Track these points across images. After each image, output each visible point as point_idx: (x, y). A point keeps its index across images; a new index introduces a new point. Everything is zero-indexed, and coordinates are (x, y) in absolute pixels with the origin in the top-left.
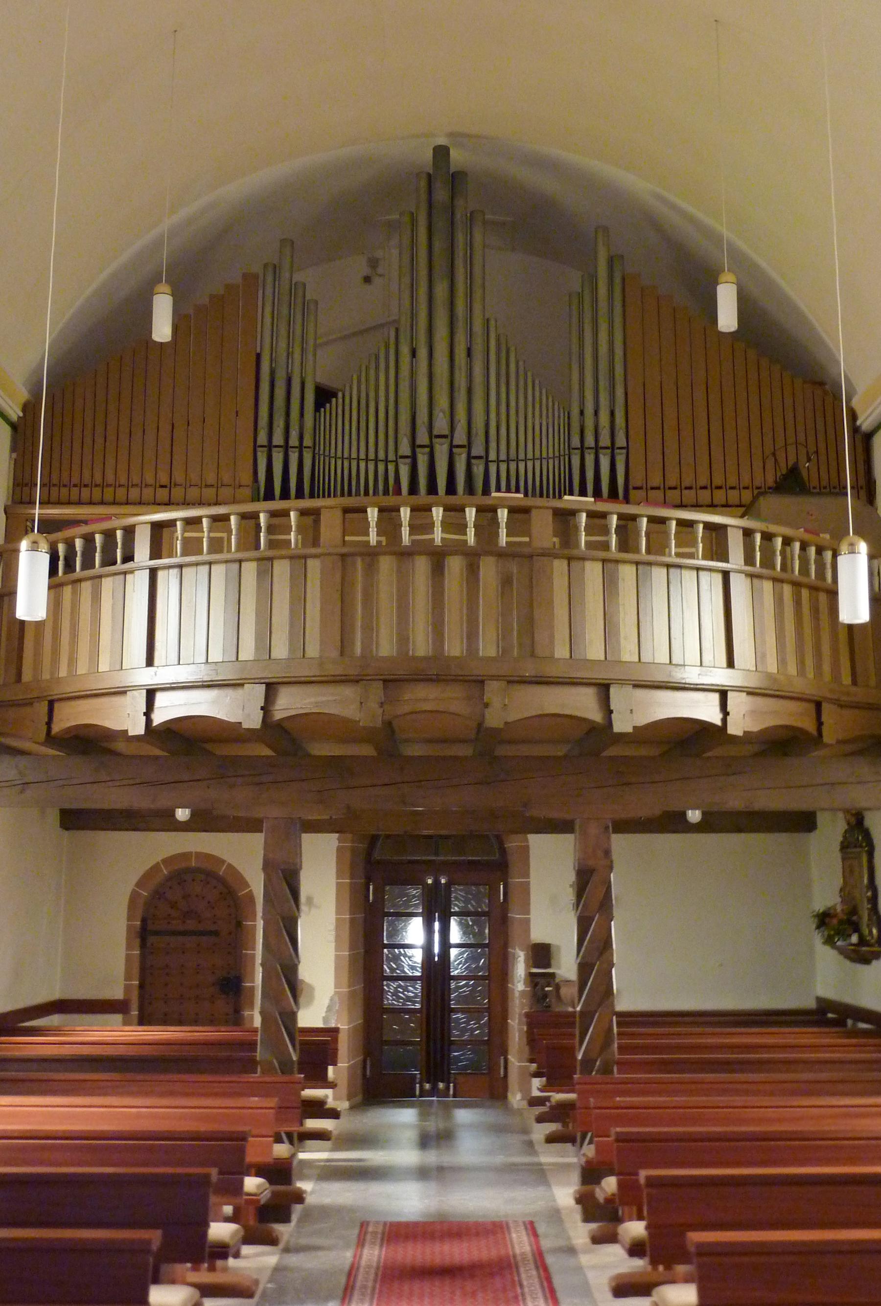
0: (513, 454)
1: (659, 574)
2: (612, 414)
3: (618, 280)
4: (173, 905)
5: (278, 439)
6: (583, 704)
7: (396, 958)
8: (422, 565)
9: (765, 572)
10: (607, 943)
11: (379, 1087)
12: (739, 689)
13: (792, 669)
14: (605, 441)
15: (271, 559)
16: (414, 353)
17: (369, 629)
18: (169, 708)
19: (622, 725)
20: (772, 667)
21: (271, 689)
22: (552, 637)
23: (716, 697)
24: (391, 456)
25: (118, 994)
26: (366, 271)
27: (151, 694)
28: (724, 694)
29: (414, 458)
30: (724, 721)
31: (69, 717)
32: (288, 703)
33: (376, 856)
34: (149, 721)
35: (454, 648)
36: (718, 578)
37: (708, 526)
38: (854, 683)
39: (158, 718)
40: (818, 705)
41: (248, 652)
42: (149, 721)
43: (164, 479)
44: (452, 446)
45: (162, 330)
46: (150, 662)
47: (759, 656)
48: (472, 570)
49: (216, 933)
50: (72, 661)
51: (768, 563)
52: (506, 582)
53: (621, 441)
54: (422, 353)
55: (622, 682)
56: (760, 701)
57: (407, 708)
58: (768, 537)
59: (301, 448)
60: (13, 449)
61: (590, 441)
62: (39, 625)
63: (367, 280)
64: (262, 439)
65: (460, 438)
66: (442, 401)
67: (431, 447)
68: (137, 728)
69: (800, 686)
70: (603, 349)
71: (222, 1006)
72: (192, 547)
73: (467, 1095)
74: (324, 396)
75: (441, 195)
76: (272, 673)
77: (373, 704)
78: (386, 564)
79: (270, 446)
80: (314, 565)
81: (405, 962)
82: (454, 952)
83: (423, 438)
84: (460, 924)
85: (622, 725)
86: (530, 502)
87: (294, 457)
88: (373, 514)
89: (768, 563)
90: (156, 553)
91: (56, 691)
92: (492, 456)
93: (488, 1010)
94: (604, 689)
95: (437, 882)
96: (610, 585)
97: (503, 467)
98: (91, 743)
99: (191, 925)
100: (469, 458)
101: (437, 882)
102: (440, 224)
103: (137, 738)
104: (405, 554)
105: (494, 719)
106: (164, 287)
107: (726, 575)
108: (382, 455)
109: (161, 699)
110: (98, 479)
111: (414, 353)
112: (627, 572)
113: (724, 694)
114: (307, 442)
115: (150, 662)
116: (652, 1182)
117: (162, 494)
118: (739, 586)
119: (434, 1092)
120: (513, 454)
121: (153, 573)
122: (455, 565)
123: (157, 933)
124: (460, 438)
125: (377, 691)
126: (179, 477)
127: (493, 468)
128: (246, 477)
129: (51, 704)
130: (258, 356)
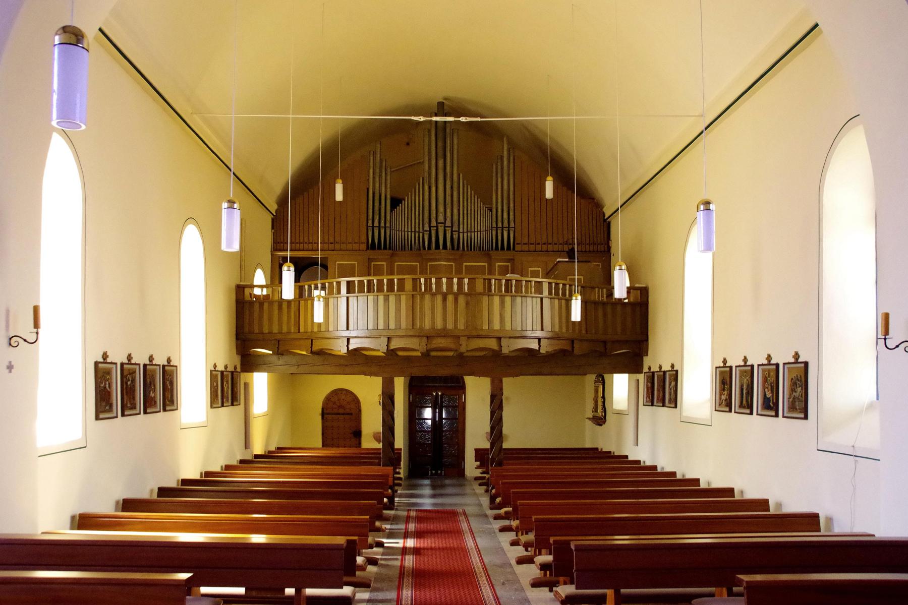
1: (519, 299)
3: (512, 158)
4: (334, 403)
5: (376, 224)
6: (492, 344)
7: (421, 424)
8: (439, 298)
11: (416, 472)
12: (545, 338)
13: (564, 330)
14: (506, 224)
16: (430, 188)
17: (422, 319)
19: (505, 351)
20: (557, 329)
21: (389, 339)
27: (348, 340)
29: (430, 231)
32: (395, 344)
35: (450, 326)
36: (539, 300)
39: (351, 348)
40: (573, 342)
41: (381, 326)
43: (332, 240)
46: (348, 329)
47: (552, 325)
48: (456, 300)
51: (557, 293)
52: (467, 303)
53: (512, 225)
55: (505, 337)
56: (553, 341)
59: (385, 227)
60: (273, 228)
61: (500, 225)
62: (289, 302)
63: (408, 144)
65: (448, 223)
66: (441, 209)
67: (437, 227)
68: (344, 350)
70: (505, 187)
72: (361, 291)
73: (447, 476)
78: (428, 297)
79: (373, 227)
81: (425, 425)
83: (434, 223)
85: (505, 351)
86: (475, 276)
87: (382, 231)
89: (557, 293)
90: (348, 292)
92: (461, 230)
94: (499, 339)
95: (437, 394)
96: (502, 303)
97: (465, 235)
99: (341, 411)
100: (452, 231)
101: (437, 394)
102: (441, 135)
104: (433, 295)
105: (463, 349)
106: (340, 181)
107: (542, 299)
109: (351, 341)
111: (430, 188)
112: (508, 299)
113: (539, 339)
114: (388, 225)
115: (348, 329)
116: (513, 493)
118: (546, 302)
119: (436, 474)
122: (450, 298)
123: (328, 414)
124: (448, 223)
125: (425, 340)
126: (337, 239)
128: (364, 239)
130: (368, 189)
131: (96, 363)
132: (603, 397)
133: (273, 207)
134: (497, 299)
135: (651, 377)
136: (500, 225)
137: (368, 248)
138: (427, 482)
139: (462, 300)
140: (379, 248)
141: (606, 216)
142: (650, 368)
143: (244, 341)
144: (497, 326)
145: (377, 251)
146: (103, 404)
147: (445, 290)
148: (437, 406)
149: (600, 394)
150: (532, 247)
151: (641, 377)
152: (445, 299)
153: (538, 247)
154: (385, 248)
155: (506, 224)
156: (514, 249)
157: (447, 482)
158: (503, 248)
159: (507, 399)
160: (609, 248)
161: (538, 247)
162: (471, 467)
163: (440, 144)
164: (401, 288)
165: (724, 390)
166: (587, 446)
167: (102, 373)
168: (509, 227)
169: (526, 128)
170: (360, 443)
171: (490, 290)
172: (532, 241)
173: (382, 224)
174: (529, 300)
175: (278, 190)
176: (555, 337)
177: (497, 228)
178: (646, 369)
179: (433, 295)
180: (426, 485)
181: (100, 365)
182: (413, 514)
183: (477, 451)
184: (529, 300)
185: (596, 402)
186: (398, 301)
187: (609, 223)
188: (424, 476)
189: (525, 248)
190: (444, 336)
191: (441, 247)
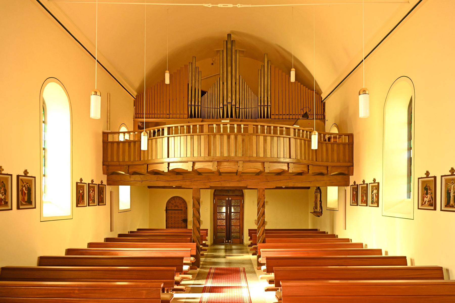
0: (245, 107)
2: (268, 98)
5: (193, 103)
8: (225, 137)
9: (298, 138)
10: (264, 213)
11: (217, 241)
12: (292, 163)
14: (266, 104)
15: (193, 135)
16: (223, 83)
18: (172, 167)
21: (194, 163)
22: (252, 152)
23: (286, 164)
24: (218, 107)
26: (212, 62)
27: (169, 164)
28: (288, 164)
30: (288, 169)
31: (151, 168)
32: (197, 166)
33: (216, 194)
34: (168, 169)
35: (233, 155)
36: (288, 139)
37: (286, 128)
38: (316, 161)
39: (170, 169)
40: (308, 166)
42: (168, 169)
44: (232, 105)
45: (167, 81)
46: (168, 157)
47: (296, 155)
49: (182, 210)
50: (152, 156)
51: (299, 136)
52: (243, 140)
53: (269, 104)
54: (225, 84)
57: (223, 167)
58: (299, 130)
60: (134, 106)
61: (262, 104)
63: (212, 64)
64: (190, 103)
65: (234, 103)
66: (230, 95)
67: (227, 105)
68: (166, 171)
69: (305, 161)
71: (183, 225)
72: (176, 133)
73: (234, 244)
74: (203, 93)
75: (229, 46)
76: (194, 160)
77: (215, 166)
78: (218, 137)
79: (191, 105)
80: (202, 137)
82: (232, 214)
83: (225, 103)
84: (234, 208)
88: (215, 126)
89: (299, 136)
90: (169, 134)
91: (148, 162)
92: (241, 107)
93: (239, 226)
94: (263, 163)
95: (229, 199)
96: (265, 141)
97: (243, 110)
98: (157, 173)
99: (176, 208)
100: (236, 108)
103: (166, 173)
104: (222, 135)
106: (168, 72)
107: (290, 138)
108: (216, 107)
110: (153, 113)
111: (223, 83)
112: (269, 138)
113: (288, 164)
114: (200, 104)
115: (168, 157)
117: (168, 116)
118: (293, 141)
119: (228, 242)
120: (245, 107)
121: (168, 138)
122: (232, 137)
123: (169, 210)
124: (234, 103)
126: (171, 112)
127: (241, 110)
128: (186, 112)
129: (148, 165)
130: (188, 84)
131: (77, 183)
132: (321, 201)
133: (135, 94)
134: (261, 138)
135: (355, 189)
136: (262, 104)
137: (188, 117)
138: (223, 247)
139: (240, 138)
140: (195, 117)
141: (323, 96)
142: (355, 182)
143: (108, 166)
144: (262, 155)
145: (193, 119)
146: (79, 200)
147: (229, 132)
148: (229, 205)
149: (319, 199)
150: (281, 117)
151: (348, 189)
152: (229, 137)
153: (284, 117)
154: (198, 117)
155: (266, 104)
156: (270, 118)
157: (234, 247)
158: (264, 117)
160: (324, 116)
161: (284, 117)
162: (247, 240)
163: (229, 58)
164: (202, 131)
166: (310, 228)
167: (79, 187)
168: (268, 105)
169: (278, 51)
170: (187, 226)
171: (257, 132)
172: (281, 113)
173: (196, 104)
174: (282, 139)
175: (137, 85)
176: (297, 163)
177: (261, 106)
178: (351, 183)
179: (222, 135)
180: (222, 249)
181: (79, 184)
182: (213, 271)
183: (249, 230)
184: (282, 139)
185: (316, 204)
186: (199, 140)
187: (324, 103)
188: (221, 243)
189: (277, 117)
190: (228, 161)
191: (229, 116)
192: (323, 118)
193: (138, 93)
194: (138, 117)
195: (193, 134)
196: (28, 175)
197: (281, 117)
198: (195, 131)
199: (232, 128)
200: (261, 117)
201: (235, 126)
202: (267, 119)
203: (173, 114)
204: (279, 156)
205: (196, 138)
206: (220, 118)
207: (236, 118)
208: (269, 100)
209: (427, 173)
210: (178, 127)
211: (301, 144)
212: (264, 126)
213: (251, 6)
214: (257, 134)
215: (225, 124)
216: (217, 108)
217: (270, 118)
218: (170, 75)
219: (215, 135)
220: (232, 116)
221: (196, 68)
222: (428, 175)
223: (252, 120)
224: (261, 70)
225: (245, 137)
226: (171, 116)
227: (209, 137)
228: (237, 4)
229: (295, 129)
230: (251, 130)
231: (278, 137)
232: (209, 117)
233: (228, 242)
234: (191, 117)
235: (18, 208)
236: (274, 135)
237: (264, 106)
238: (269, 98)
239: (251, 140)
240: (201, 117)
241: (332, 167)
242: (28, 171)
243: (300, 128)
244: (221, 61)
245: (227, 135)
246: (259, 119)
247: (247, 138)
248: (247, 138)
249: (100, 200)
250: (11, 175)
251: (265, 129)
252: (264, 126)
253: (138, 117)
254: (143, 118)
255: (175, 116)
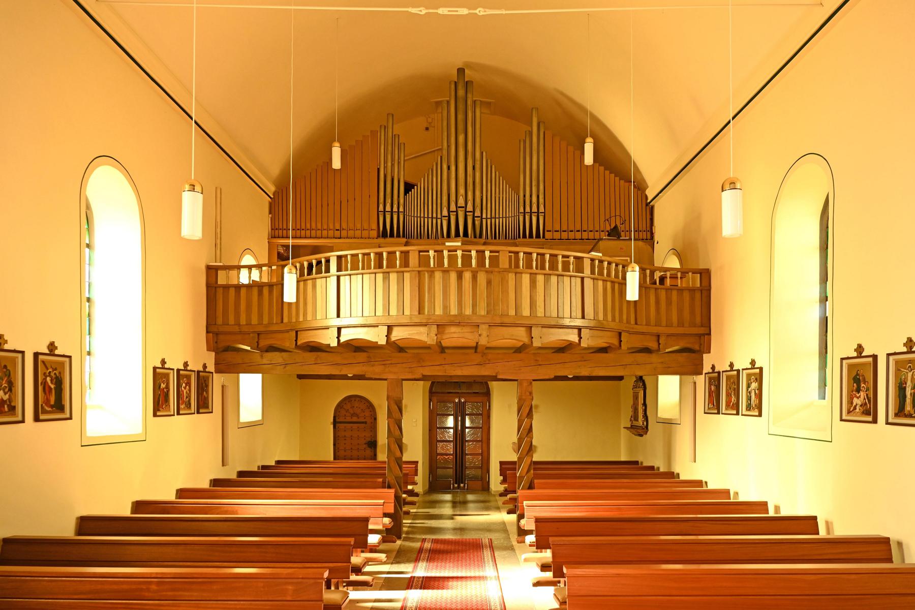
0: (493, 215)
2: (538, 197)
5: (388, 208)
8: (453, 276)
9: (600, 277)
10: (530, 430)
11: (436, 485)
12: (586, 327)
14: (535, 209)
15: (389, 273)
16: (449, 168)
18: (346, 336)
21: (390, 328)
22: (508, 307)
23: (576, 331)
24: (439, 216)
25: (907, 561)
26: (426, 125)
27: (339, 329)
28: (580, 330)
30: (580, 341)
31: (304, 339)
32: (397, 334)
33: (434, 390)
34: (339, 340)
35: (468, 311)
36: (579, 280)
37: (575, 257)
38: (636, 324)
39: (343, 339)
40: (620, 334)
42: (339, 340)
44: (466, 212)
45: (336, 164)
46: (338, 316)
47: (596, 312)
49: (366, 423)
50: (305, 314)
51: (601, 273)
52: (489, 283)
53: (542, 209)
54: (453, 168)
57: (448, 336)
58: (601, 262)
60: (270, 213)
61: (528, 209)
63: (427, 129)
64: (381, 208)
65: (470, 207)
66: (462, 191)
67: (457, 212)
68: (334, 343)
69: (613, 325)
71: (369, 452)
72: (355, 267)
73: (471, 491)
74: (409, 187)
75: (461, 92)
76: (390, 322)
77: (433, 335)
78: (438, 275)
79: (385, 211)
80: (407, 276)
82: (467, 430)
83: (453, 208)
84: (470, 419)
88: (431, 253)
89: (601, 273)
90: (339, 269)
91: (298, 327)
92: (484, 216)
93: (482, 454)
94: (530, 328)
95: (460, 400)
96: (533, 283)
97: (489, 221)
98: (316, 348)
99: (355, 419)
100: (474, 217)
103: (334, 347)
104: (446, 272)
106: (337, 144)
107: (582, 279)
108: (434, 215)
110: (308, 227)
111: (449, 168)
112: (540, 279)
113: (580, 330)
114: (401, 209)
115: (338, 316)
117: (337, 233)
118: (588, 283)
119: (459, 487)
120: (493, 215)
121: (338, 278)
122: (467, 276)
123: (340, 423)
124: (470, 207)
126: (344, 226)
127: (484, 221)
128: (374, 226)
129: (297, 332)
130: (379, 170)
131: (155, 368)
132: (645, 404)
133: (271, 189)
134: (526, 278)
135: (715, 380)
136: (528, 209)
137: (378, 236)
138: (448, 497)
139: (482, 278)
140: (392, 235)
141: (650, 194)
142: (713, 367)
143: (217, 334)
144: (526, 312)
145: (389, 240)
147: (460, 265)
148: (460, 413)
149: (641, 401)
150: (564, 235)
151: (701, 380)
152: (460, 276)
153: (571, 235)
154: (398, 236)
155: (535, 209)
156: (544, 237)
157: (470, 497)
158: (531, 236)
159: (406, 406)
160: (652, 234)
161: (571, 235)
162: (496, 482)
163: (461, 117)
164: (405, 263)
165: (858, 390)
166: (623, 459)
168: (538, 212)
169: (559, 104)
170: (375, 455)
171: (517, 266)
172: (564, 228)
173: (395, 209)
174: (567, 280)
175: (275, 171)
176: (598, 328)
177: (524, 213)
178: (707, 368)
179: (446, 272)
180: (447, 502)
181: (158, 370)
183: (502, 463)
184: (567, 280)
185: (635, 410)
186: (401, 282)
187: (652, 207)
188: (445, 489)
189: (557, 235)
190: (458, 324)
191: (461, 234)
192: (649, 237)
193: (277, 186)
194: (277, 235)
195: (388, 270)
196: (57, 352)
197: (564, 235)
198: (391, 264)
199: (467, 259)
200: (524, 236)
201: (474, 253)
202: (538, 240)
203: (348, 230)
204: (561, 315)
205: (393, 277)
206: (443, 237)
207: (475, 237)
208: (541, 200)
209: (860, 349)
210: (357, 255)
211: (605, 289)
212: (531, 254)
213: (504, 12)
214: (518, 270)
215: (452, 250)
216: (437, 218)
217: (544, 237)
218: (342, 151)
219: (433, 272)
220: (466, 234)
221: (394, 136)
222: (861, 353)
223: (507, 241)
224: (525, 142)
225: (492, 276)
226: (344, 233)
227: (419, 276)
228: (476, 9)
229: (592, 260)
230: (504, 262)
231: (558, 275)
232: (420, 236)
233: (459, 487)
234: (384, 235)
235: (37, 419)
236: (551, 272)
237: (531, 213)
238: (541, 197)
239: (504, 282)
240: (404, 236)
241: (669, 336)
242: (56, 344)
243: (603, 258)
244: (445, 123)
245: (457, 272)
246: (522, 239)
247: (496, 279)
248: (496, 279)
249: (201, 403)
250: (23, 352)
251: (532, 260)
252: (531, 254)
253: (277, 235)
254: (288, 237)
255: (351, 233)
